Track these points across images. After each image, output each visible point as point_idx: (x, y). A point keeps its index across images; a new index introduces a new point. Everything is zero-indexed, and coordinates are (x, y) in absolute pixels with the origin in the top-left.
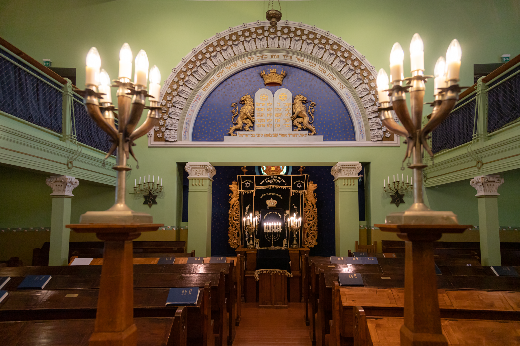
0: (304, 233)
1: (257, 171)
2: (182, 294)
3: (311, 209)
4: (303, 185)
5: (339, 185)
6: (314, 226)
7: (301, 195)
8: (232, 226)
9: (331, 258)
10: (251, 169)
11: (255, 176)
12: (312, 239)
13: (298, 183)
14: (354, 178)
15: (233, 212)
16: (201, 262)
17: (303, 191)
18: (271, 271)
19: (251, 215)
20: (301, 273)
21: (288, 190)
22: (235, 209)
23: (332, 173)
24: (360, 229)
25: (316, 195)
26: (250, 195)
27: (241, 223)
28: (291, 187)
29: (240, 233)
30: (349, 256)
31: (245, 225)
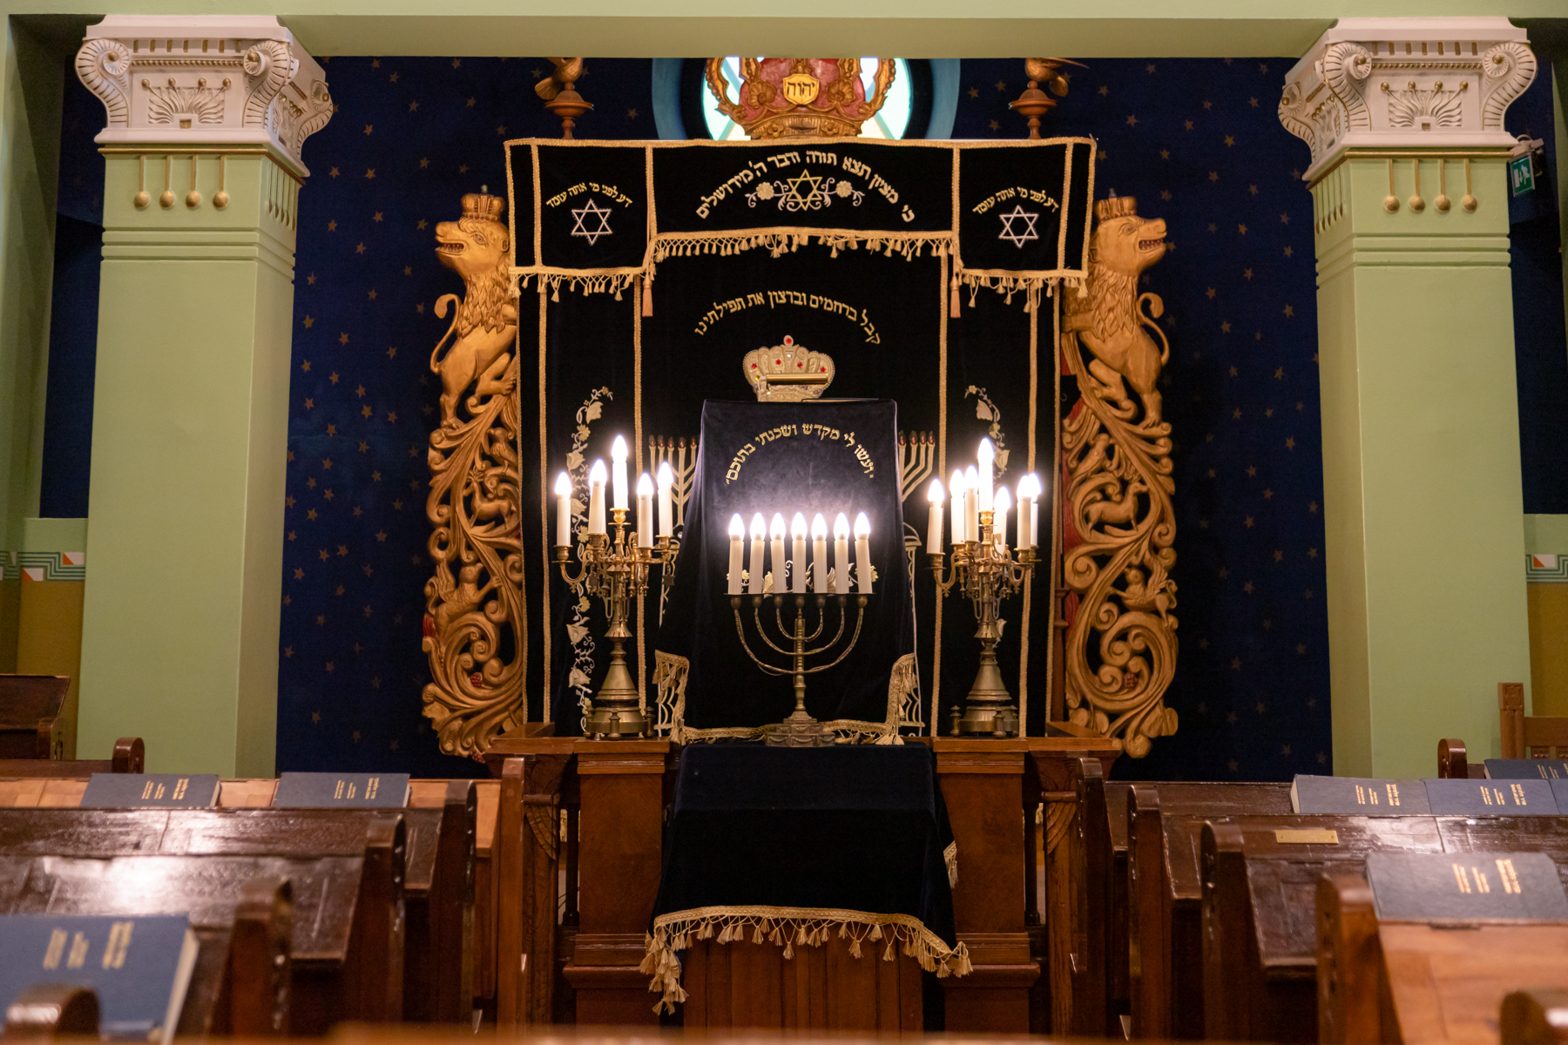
0: (1064, 634)
1: (664, 110)
2: (50, 961)
3: (1120, 432)
4: (1048, 221)
5: (1356, 213)
6: (1146, 572)
7: (1032, 307)
8: (456, 566)
9: (1301, 792)
10: (620, 87)
11: (649, 145)
12: (1130, 680)
13: (1008, 206)
14: (1474, 155)
15: (460, 453)
16: (201, 797)
17: (1053, 275)
18: (789, 927)
19: (620, 447)
20: (1040, 948)
21: (927, 264)
22: (481, 425)
23: (1293, 117)
24: (1534, 588)
25: (1157, 307)
26: (615, 310)
27: (534, 517)
28: (947, 242)
29: (521, 627)
30: (1443, 771)
31: (565, 539)
